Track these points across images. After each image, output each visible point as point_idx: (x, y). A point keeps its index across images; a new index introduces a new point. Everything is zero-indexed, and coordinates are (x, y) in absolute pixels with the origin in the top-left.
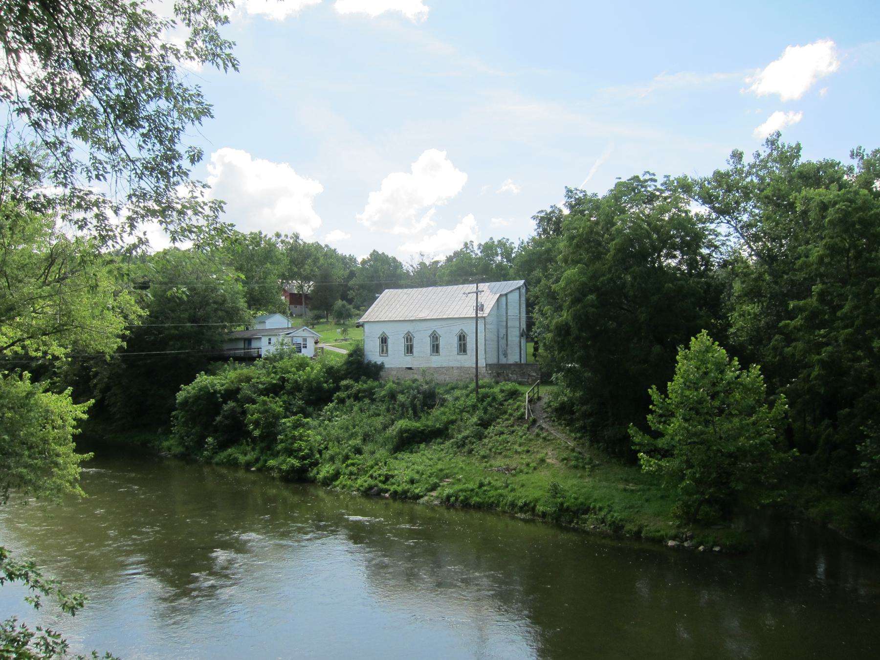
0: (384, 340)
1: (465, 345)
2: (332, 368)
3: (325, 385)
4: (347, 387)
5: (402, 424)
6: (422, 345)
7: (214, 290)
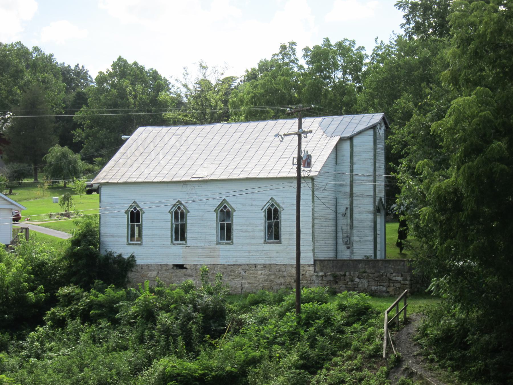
0: (135, 217)
3: (31, 295)
4: (69, 299)
6: (202, 225)
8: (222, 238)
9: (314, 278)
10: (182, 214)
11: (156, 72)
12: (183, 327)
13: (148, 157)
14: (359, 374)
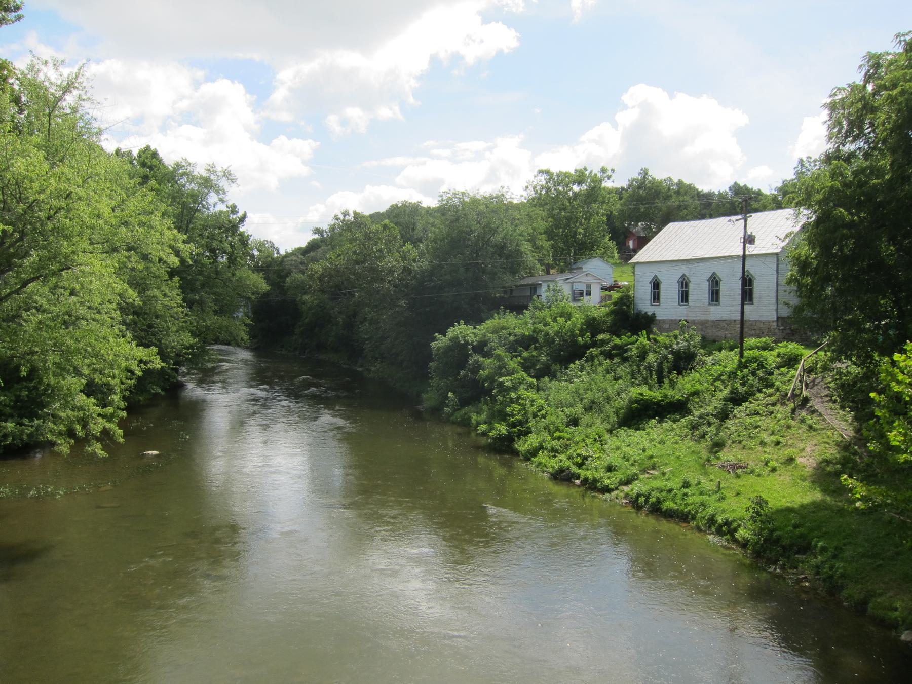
0: (656, 285)
1: (717, 292)
2: (594, 319)
3: (580, 339)
4: (603, 342)
5: (635, 392)
6: (699, 291)
7: (494, 231)
8: (712, 301)
9: (777, 331)
10: (686, 284)
11: (759, 190)
12: (660, 365)
13: (675, 243)
14: (771, 408)
